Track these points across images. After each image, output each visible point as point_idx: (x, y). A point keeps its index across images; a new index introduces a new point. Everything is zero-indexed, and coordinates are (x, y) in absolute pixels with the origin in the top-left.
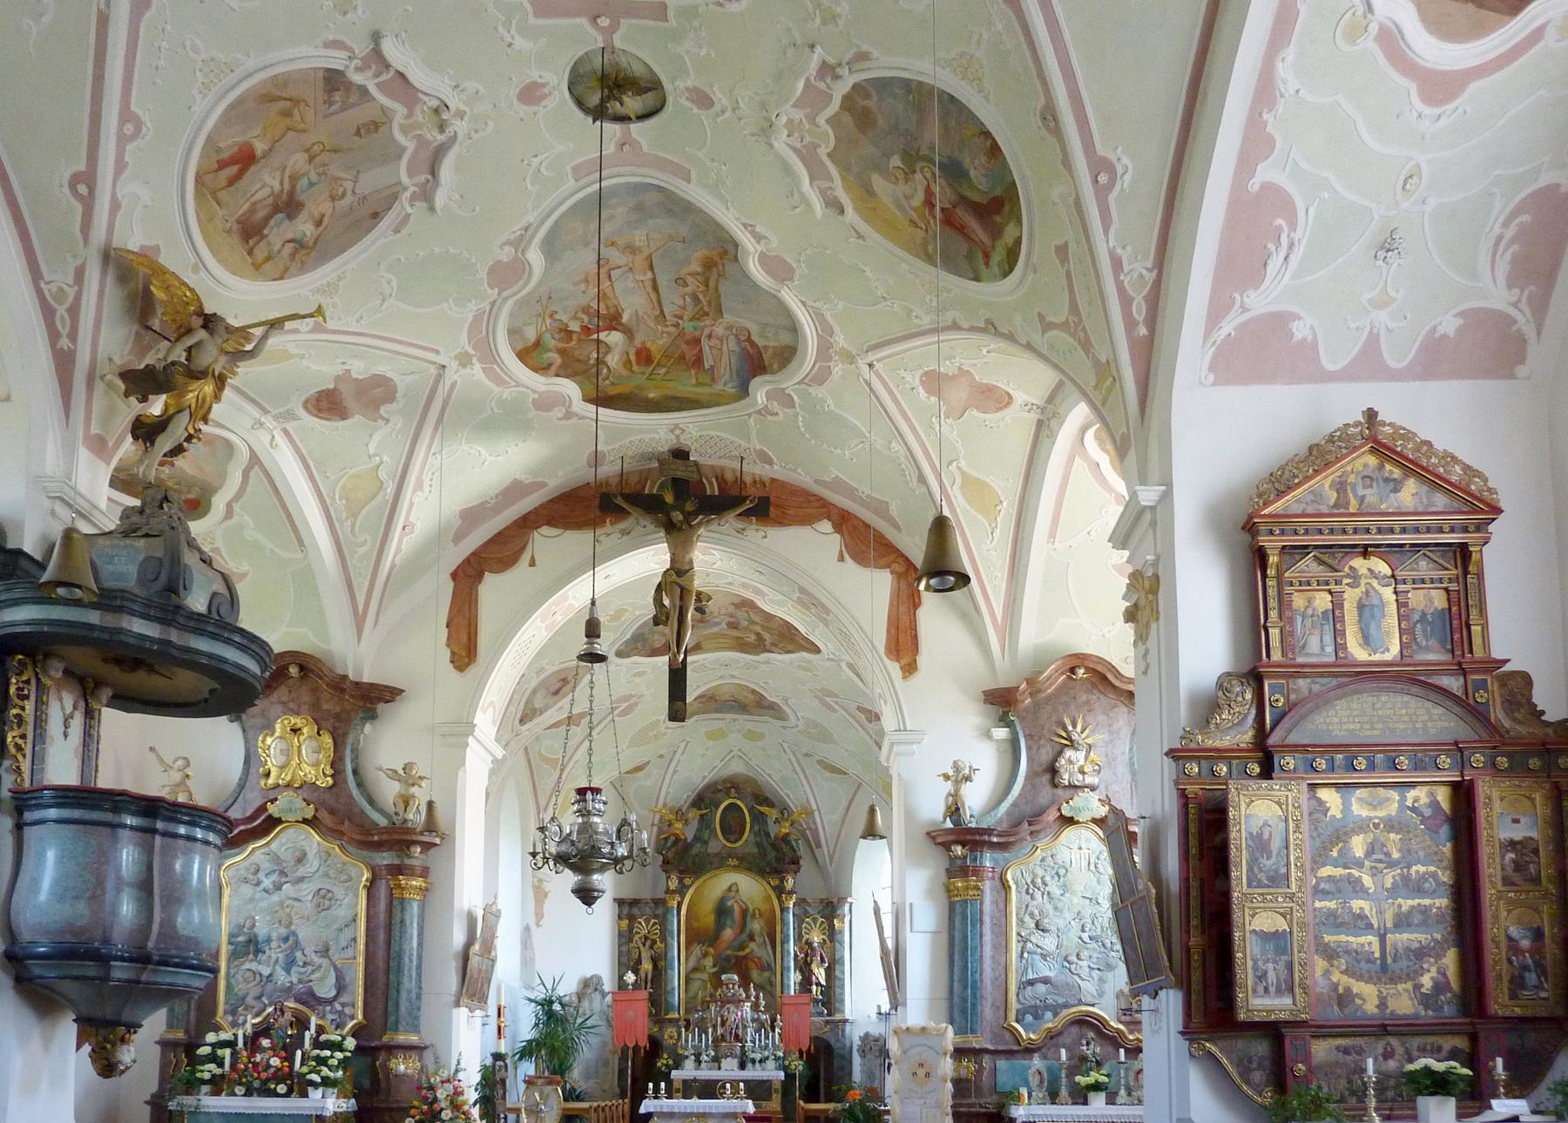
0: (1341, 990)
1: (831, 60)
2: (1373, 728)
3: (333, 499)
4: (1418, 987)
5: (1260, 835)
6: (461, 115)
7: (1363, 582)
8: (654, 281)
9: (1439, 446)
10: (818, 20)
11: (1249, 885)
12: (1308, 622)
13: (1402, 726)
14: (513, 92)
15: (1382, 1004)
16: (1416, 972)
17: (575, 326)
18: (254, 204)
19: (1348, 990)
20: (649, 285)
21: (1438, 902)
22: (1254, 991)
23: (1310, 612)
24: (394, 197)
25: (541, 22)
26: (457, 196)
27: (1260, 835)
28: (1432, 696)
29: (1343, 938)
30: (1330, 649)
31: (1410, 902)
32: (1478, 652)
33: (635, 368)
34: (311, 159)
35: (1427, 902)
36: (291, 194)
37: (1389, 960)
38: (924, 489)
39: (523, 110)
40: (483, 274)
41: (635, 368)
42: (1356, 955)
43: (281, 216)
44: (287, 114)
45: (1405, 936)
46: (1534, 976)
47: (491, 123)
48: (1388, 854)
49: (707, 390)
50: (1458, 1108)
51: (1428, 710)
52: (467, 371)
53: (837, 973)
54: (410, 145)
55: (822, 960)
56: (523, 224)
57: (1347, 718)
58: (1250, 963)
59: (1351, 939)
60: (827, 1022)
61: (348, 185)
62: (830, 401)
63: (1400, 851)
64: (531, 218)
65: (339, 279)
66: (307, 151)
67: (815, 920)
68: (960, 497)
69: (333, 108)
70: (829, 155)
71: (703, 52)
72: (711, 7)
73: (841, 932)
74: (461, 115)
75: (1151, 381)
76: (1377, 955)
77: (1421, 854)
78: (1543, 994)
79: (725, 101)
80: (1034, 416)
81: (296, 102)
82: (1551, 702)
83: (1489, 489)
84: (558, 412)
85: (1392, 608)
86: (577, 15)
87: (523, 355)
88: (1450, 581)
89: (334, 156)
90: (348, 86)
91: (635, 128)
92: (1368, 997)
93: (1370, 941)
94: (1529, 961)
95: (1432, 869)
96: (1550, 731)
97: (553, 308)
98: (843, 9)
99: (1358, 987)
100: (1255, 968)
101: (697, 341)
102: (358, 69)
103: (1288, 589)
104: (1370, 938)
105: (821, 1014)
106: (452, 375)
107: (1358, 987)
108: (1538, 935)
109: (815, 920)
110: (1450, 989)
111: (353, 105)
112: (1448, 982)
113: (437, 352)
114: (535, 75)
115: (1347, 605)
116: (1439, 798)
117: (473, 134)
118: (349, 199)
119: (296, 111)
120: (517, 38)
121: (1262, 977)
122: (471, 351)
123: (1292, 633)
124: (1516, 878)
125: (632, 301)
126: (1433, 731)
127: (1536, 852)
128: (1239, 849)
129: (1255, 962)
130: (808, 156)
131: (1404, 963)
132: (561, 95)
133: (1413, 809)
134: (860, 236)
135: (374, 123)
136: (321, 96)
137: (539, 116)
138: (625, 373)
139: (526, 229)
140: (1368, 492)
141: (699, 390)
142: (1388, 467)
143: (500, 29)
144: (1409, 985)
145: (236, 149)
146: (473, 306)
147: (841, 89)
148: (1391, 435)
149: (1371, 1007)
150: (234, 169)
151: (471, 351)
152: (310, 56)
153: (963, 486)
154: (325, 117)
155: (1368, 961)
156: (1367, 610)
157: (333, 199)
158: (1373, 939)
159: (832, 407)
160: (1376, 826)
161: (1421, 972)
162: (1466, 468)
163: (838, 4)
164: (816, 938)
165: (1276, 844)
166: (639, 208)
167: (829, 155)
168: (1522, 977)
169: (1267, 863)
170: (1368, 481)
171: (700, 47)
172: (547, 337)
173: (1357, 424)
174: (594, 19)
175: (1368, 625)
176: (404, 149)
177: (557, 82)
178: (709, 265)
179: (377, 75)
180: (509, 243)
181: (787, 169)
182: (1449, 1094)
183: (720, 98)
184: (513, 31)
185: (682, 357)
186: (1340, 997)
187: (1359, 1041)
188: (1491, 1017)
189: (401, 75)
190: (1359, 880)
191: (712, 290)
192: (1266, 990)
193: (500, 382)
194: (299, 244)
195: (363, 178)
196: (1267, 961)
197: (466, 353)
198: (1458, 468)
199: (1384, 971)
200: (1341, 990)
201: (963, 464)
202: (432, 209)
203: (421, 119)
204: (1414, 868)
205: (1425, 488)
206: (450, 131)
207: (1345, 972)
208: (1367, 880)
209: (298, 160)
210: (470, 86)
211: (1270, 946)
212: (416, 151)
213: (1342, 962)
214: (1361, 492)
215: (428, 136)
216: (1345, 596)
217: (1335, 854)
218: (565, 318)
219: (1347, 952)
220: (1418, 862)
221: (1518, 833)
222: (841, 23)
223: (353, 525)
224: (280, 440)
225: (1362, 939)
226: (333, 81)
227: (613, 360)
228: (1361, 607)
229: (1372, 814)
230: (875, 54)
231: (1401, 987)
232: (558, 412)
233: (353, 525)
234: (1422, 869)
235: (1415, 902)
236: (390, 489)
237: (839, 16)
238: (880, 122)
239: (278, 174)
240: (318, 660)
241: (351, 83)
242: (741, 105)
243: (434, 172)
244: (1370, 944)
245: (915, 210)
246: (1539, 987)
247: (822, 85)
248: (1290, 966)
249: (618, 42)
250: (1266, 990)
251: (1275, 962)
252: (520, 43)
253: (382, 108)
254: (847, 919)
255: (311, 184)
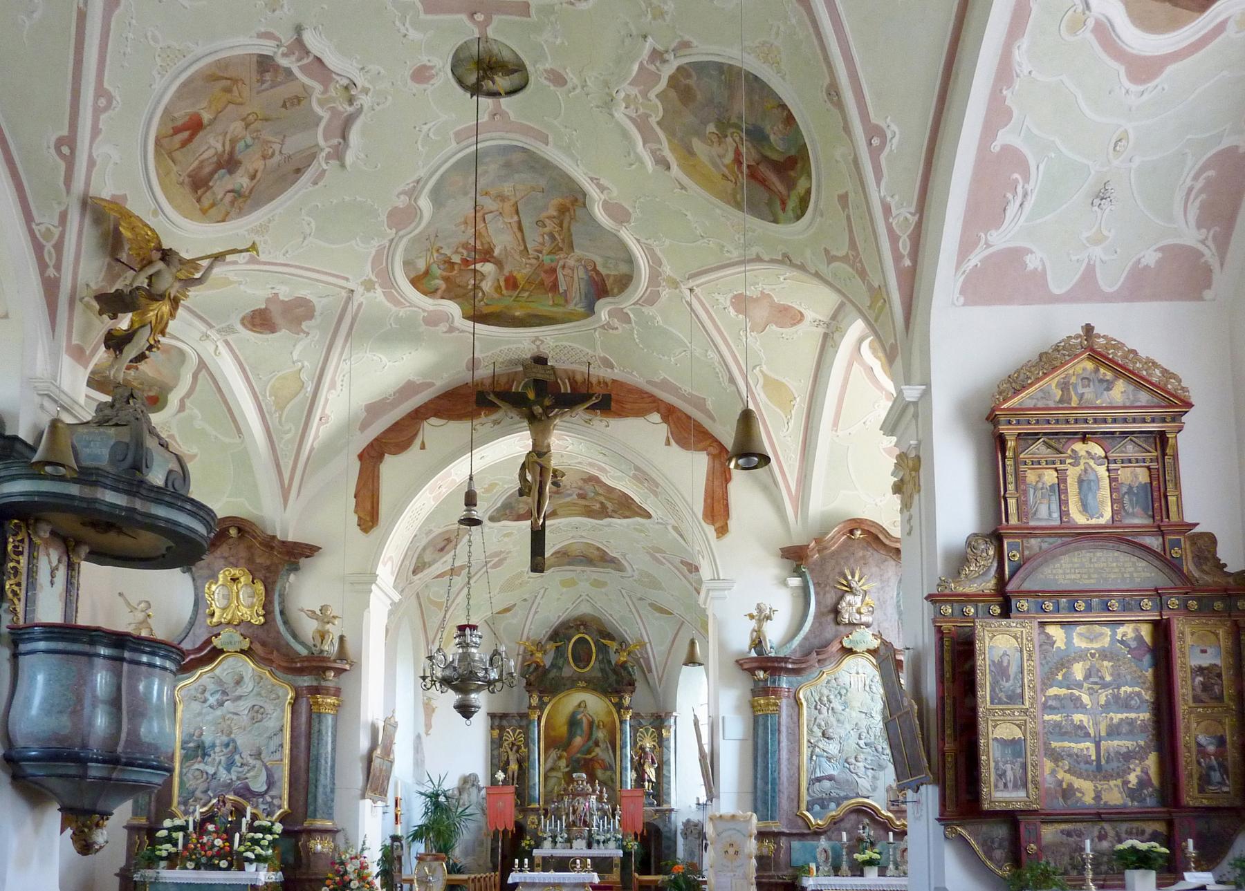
0: (1065, 786)
1: (660, 48)
2: (1090, 578)
3: (264, 396)
4: (1126, 783)
5: (1000, 663)
6: (366, 91)
7: (1082, 461)
8: (519, 223)
9: (1143, 354)
10: (650, 16)
11: (992, 703)
12: (1039, 494)
13: (1113, 576)
14: (408, 73)
15: (1098, 797)
16: (1124, 771)
17: (456, 259)
18: (202, 162)
19: (1070, 785)
20: (515, 226)
21: (1142, 716)
22: (996, 786)
23: (1040, 485)
24: (313, 156)
25: (429, 17)
26: (363, 156)
27: (1000, 663)
28: (1137, 552)
29: (1066, 744)
30: (1056, 515)
31: (1120, 716)
32: (1174, 517)
33: (504, 292)
34: (247, 126)
35: (1133, 715)
36: (231, 154)
37: (1103, 762)
38: (733, 388)
39: (416, 87)
40: (383, 217)
41: (504, 292)
42: (1077, 758)
43: (223, 171)
44: (228, 90)
45: (1116, 743)
46: (1218, 774)
47: (390, 98)
48: (1102, 678)
49: (561, 309)
50: (1158, 879)
51: (1134, 563)
52: (371, 294)
53: (665, 772)
54: (325, 115)
55: (653, 762)
56: (415, 177)
57: (1069, 570)
58: (992, 764)
59: (1073, 745)
60: (657, 811)
61: (277, 147)
62: (659, 318)
63: (1111, 675)
64: (422, 173)
65: (269, 221)
66: (243, 120)
67: (647, 730)
68: (762, 394)
69: (265, 86)
70: (658, 123)
71: (559, 41)
72: (565, 5)
73: (668, 739)
74: (366, 91)
75: (914, 302)
76: (1094, 758)
77: (1129, 677)
78: (1225, 789)
79: (575, 80)
80: (821, 330)
81: (235, 81)
82: (1232, 557)
83: (1183, 388)
84: (443, 327)
85: (1105, 482)
86: (458, 12)
87: (416, 282)
88: (1152, 461)
89: (265, 123)
90: (277, 68)
91: (504, 101)
92: (1086, 791)
93: (1087, 747)
94: (1214, 763)
95: (1137, 689)
96: (1231, 580)
97: (439, 244)
98: (670, 7)
99: (1078, 783)
100: (997, 768)
101: (553, 271)
102: (284, 55)
103: (1022, 467)
104: (1088, 744)
105: (652, 805)
106: (359, 298)
107: (1078, 783)
108: (1221, 741)
109: (647, 730)
110: (1152, 785)
111: (280, 84)
112: (1150, 779)
113: (347, 279)
114: (424, 59)
115: (1069, 480)
116: (1143, 633)
117: (376, 107)
118: (277, 158)
119: (235, 88)
120: (411, 30)
121: (1002, 775)
122: (374, 279)
123: (1026, 503)
124: (1204, 696)
125: (502, 239)
126: (1138, 580)
127: (1219, 676)
128: (984, 674)
129: (997, 763)
130: (641, 124)
131: (1115, 764)
132: (445, 76)
133: (1122, 642)
134: (683, 187)
135: (297, 97)
136: (255, 76)
137: (428, 92)
138: (496, 296)
139: (418, 182)
140: (1086, 390)
141: (555, 309)
142: (1102, 370)
143: (397, 23)
144: (1119, 782)
145: (187, 118)
146: (375, 243)
147: (667, 71)
148: (1105, 345)
149: (1089, 799)
150: (186, 134)
151: (374, 279)
152: (246, 44)
153: (764, 386)
154: (258, 93)
155: (1087, 762)
156: (1085, 484)
157: (264, 158)
158: (1090, 745)
159: (661, 323)
160: (1093, 655)
161: (1128, 771)
162: (1164, 371)
163: (665, 3)
164: (648, 744)
165: (1013, 670)
166: (507, 165)
167: (658, 123)
168: (1208, 776)
169: (1006, 685)
170: (1086, 382)
171: (556, 37)
172: (434, 267)
173: (1078, 336)
174: (472, 15)
175: (1086, 496)
176: (320, 118)
177: (442, 65)
178: (563, 210)
179: (299, 60)
180: (404, 193)
181: (625, 134)
182: (1150, 868)
183: (572, 78)
184: (407, 25)
185: (542, 284)
186: (1064, 791)
187: (1079, 826)
188: (1184, 807)
189: (319, 60)
190: (1079, 698)
191: (565, 230)
192: (1005, 785)
193: (397, 303)
194: (237, 194)
195: (288, 141)
196: (1006, 763)
197: (370, 280)
198: (1157, 372)
199: (1099, 771)
200: (1065, 786)
201: (764, 368)
202: (343, 166)
203: (334, 94)
204: (1123, 689)
205: (1131, 387)
206: (357, 104)
207: (1068, 771)
208: (1086, 699)
209: (236, 127)
210: (374, 68)
211: (1009, 751)
212: (330, 120)
213: (1066, 764)
214: (1080, 390)
215: (340, 108)
216: (1068, 473)
217: (1060, 677)
218: (448, 253)
219: (1070, 755)
220: (1126, 684)
221: (1205, 661)
222: (668, 18)
223: (280, 417)
224: (223, 349)
225: (1082, 745)
226: (265, 64)
227: (487, 286)
228: (1081, 482)
229: (1090, 646)
230: (695, 43)
231: (1112, 783)
232: (443, 327)
233: (280, 417)
234: (1129, 690)
235: (1124, 716)
236: (310, 388)
237: (667, 13)
238: (699, 97)
239: (221, 138)
240: (253, 524)
241: (278, 66)
242: (589, 83)
243: (344, 137)
244: (1088, 749)
245: (726, 166)
246: (1222, 783)
247: (652, 68)
248: (1024, 767)
249: (490, 33)
250: (1005, 785)
251: (1012, 763)
252: (413, 34)
253: (304, 86)
254: (672, 729)
255: (247, 146)
